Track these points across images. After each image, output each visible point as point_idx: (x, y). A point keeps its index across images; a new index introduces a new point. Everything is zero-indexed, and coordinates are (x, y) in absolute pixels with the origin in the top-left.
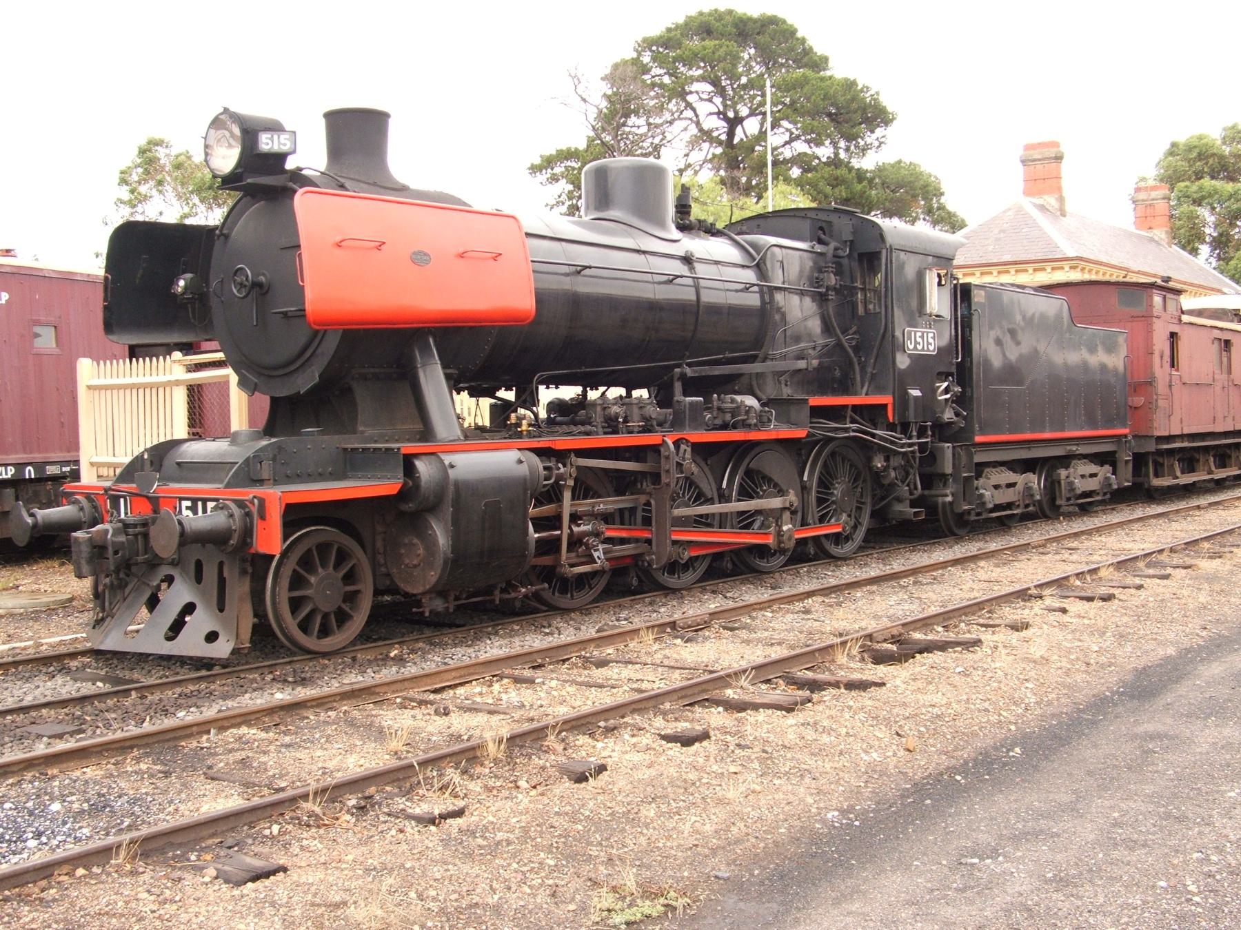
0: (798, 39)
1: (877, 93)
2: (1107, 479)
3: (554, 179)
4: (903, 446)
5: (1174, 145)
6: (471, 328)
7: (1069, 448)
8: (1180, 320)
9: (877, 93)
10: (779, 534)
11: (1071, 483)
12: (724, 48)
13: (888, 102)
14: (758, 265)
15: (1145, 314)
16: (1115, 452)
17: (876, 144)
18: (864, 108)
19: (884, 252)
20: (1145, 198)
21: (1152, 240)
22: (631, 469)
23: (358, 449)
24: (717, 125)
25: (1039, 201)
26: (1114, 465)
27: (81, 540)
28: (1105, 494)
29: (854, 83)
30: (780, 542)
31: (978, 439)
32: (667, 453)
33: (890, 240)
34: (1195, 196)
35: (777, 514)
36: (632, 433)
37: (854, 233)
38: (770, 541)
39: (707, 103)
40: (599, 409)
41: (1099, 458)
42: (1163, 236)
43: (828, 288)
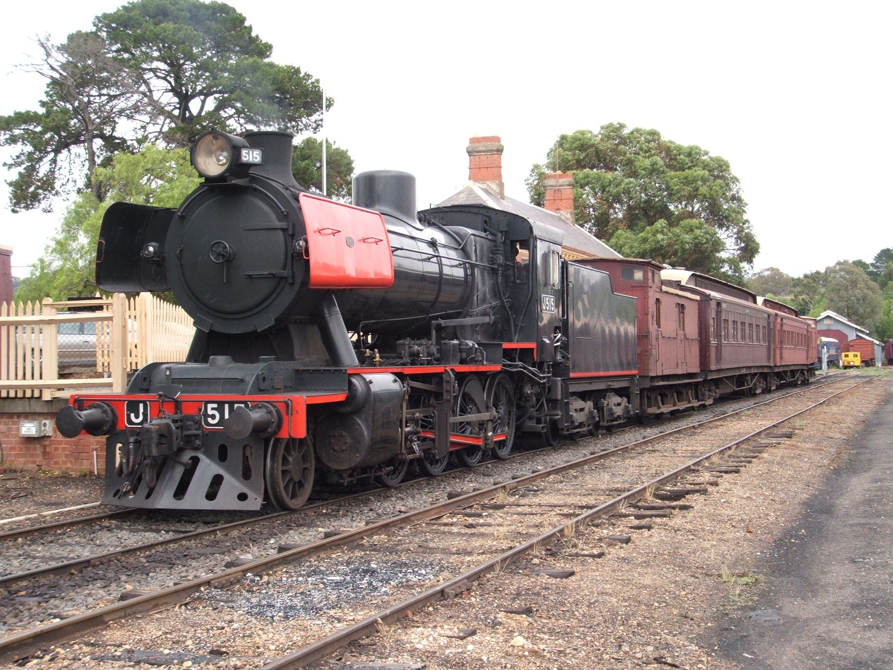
0: (246, 27)
1: (318, 81)
2: (591, 412)
3: (13, 140)
4: (541, 378)
5: (563, 138)
6: (351, 290)
7: (609, 383)
8: (661, 290)
9: (318, 81)
10: (486, 438)
11: (611, 409)
12: (183, 32)
13: (327, 90)
14: (463, 249)
15: (643, 285)
16: (628, 388)
17: (314, 125)
18: (306, 93)
19: (532, 240)
20: (554, 184)
21: (560, 219)
22: (420, 387)
23: (309, 370)
24: (169, 100)
25: (484, 186)
26: (628, 397)
27: (153, 430)
28: (589, 425)
29: (298, 71)
30: (486, 445)
31: (572, 375)
32: (448, 379)
33: (536, 232)
34: (582, 182)
35: (482, 425)
36: (423, 364)
37: (508, 225)
38: (481, 443)
39: (162, 81)
40: (407, 347)
41: (621, 392)
42: (569, 216)
43: (499, 265)
